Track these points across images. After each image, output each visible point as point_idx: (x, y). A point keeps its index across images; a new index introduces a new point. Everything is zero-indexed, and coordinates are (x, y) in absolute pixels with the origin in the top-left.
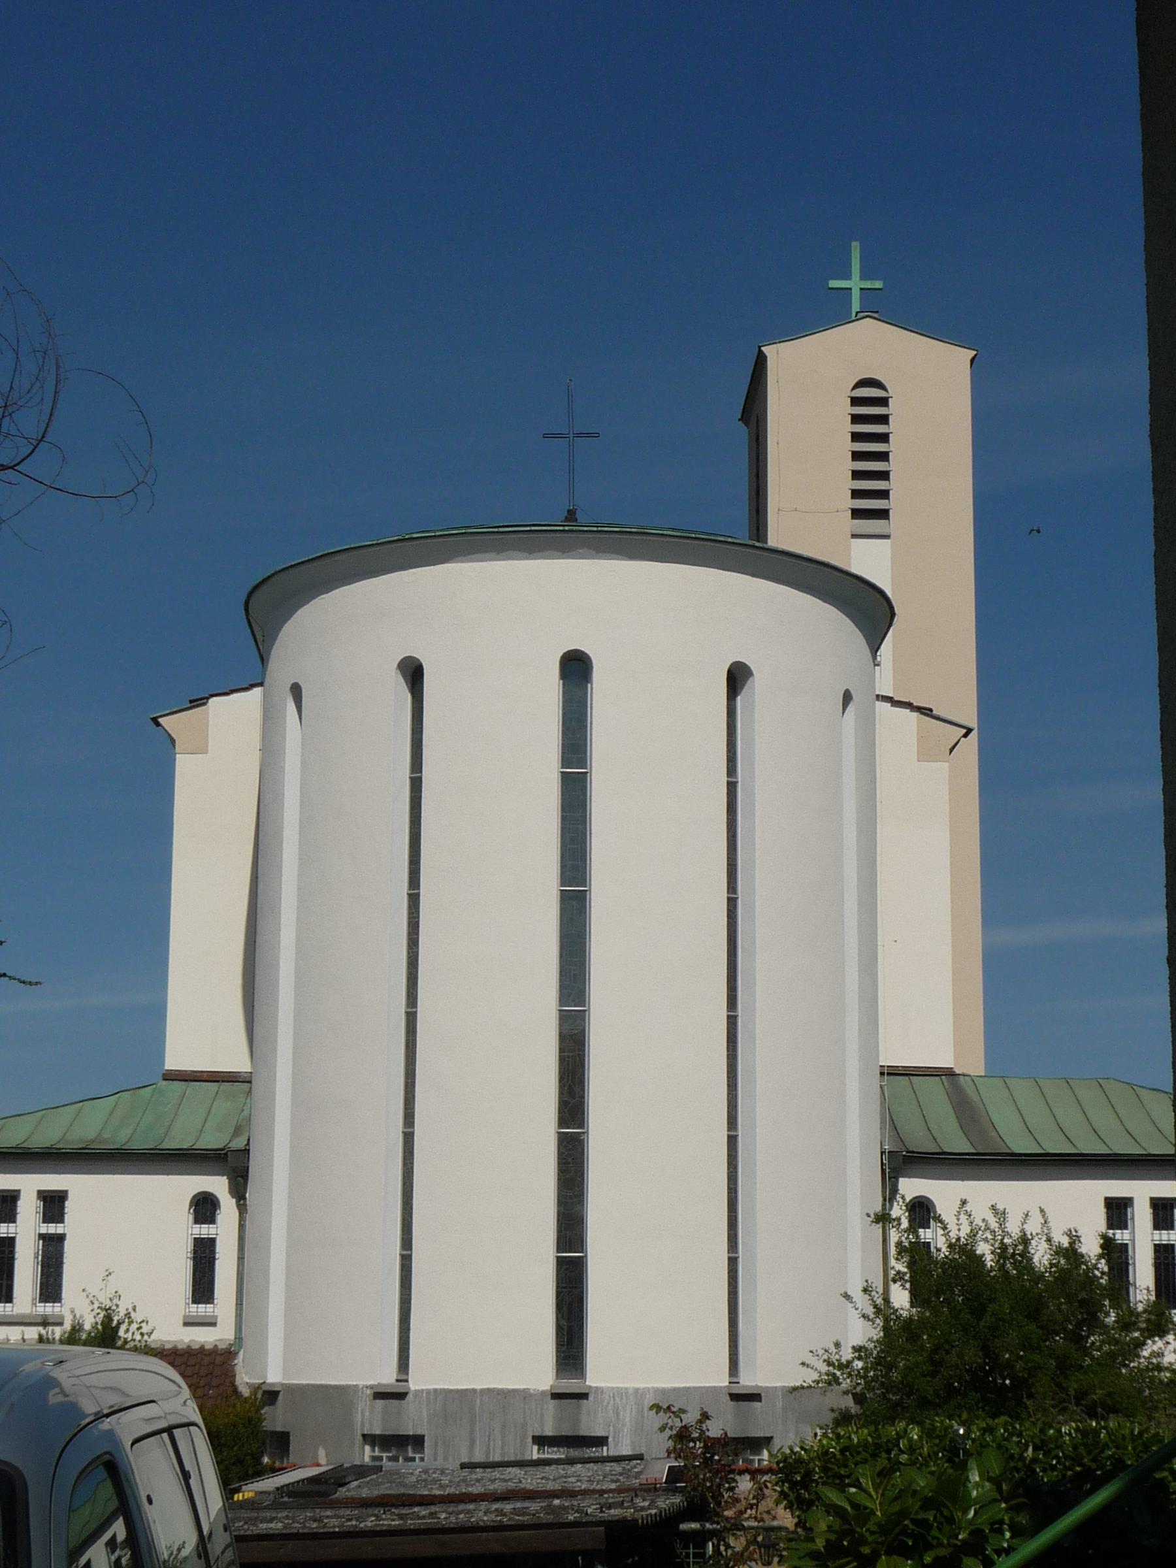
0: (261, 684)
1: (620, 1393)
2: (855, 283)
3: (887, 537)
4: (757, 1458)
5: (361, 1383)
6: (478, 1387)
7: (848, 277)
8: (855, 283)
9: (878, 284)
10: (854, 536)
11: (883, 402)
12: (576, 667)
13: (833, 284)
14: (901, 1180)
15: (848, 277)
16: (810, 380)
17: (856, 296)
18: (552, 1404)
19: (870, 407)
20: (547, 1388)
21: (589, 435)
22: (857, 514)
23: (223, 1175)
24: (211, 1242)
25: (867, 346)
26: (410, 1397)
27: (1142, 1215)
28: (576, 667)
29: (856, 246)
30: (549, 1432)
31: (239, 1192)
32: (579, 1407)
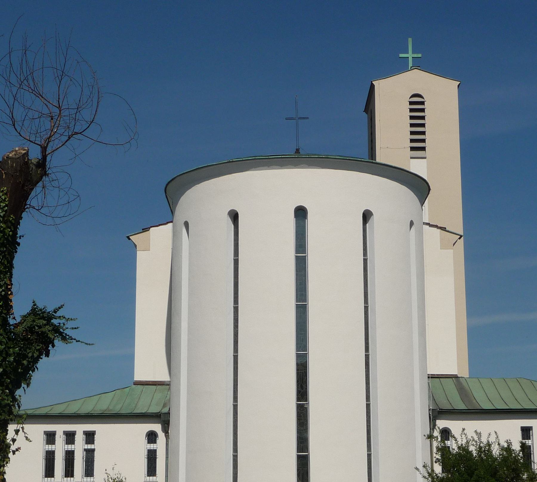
0: (172, 222)
3: (425, 158)
8: (410, 55)
9: (420, 55)
10: (411, 158)
11: (423, 103)
12: (301, 213)
13: (401, 55)
16: (392, 94)
17: (410, 60)
19: (417, 105)
21: (304, 118)
25: (415, 80)
28: (301, 213)
29: (410, 40)
31: (166, 430)
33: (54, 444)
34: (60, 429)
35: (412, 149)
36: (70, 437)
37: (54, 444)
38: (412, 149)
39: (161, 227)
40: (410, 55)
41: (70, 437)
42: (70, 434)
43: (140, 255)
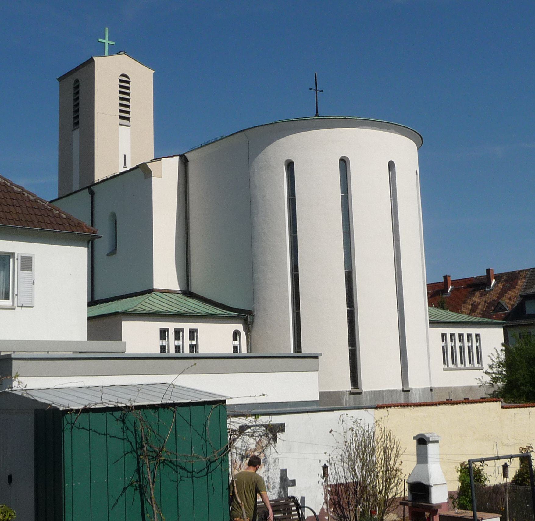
1: (416, 389)
2: (107, 41)
3: (129, 126)
5: (344, 390)
6: (384, 389)
7: (109, 40)
9: (113, 43)
10: (120, 125)
12: (391, 165)
18: (403, 393)
19: (125, 83)
22: (121, 117)
23: (121, 323)
25: (123, 63)
26: (363, 394)
28: (391, 165)
29: (107, 29)
31: (248, 331)
34: (172, 326)
39: (169, 158)
40: (107, 41)
41: (178, 333)
43: (155, 180)
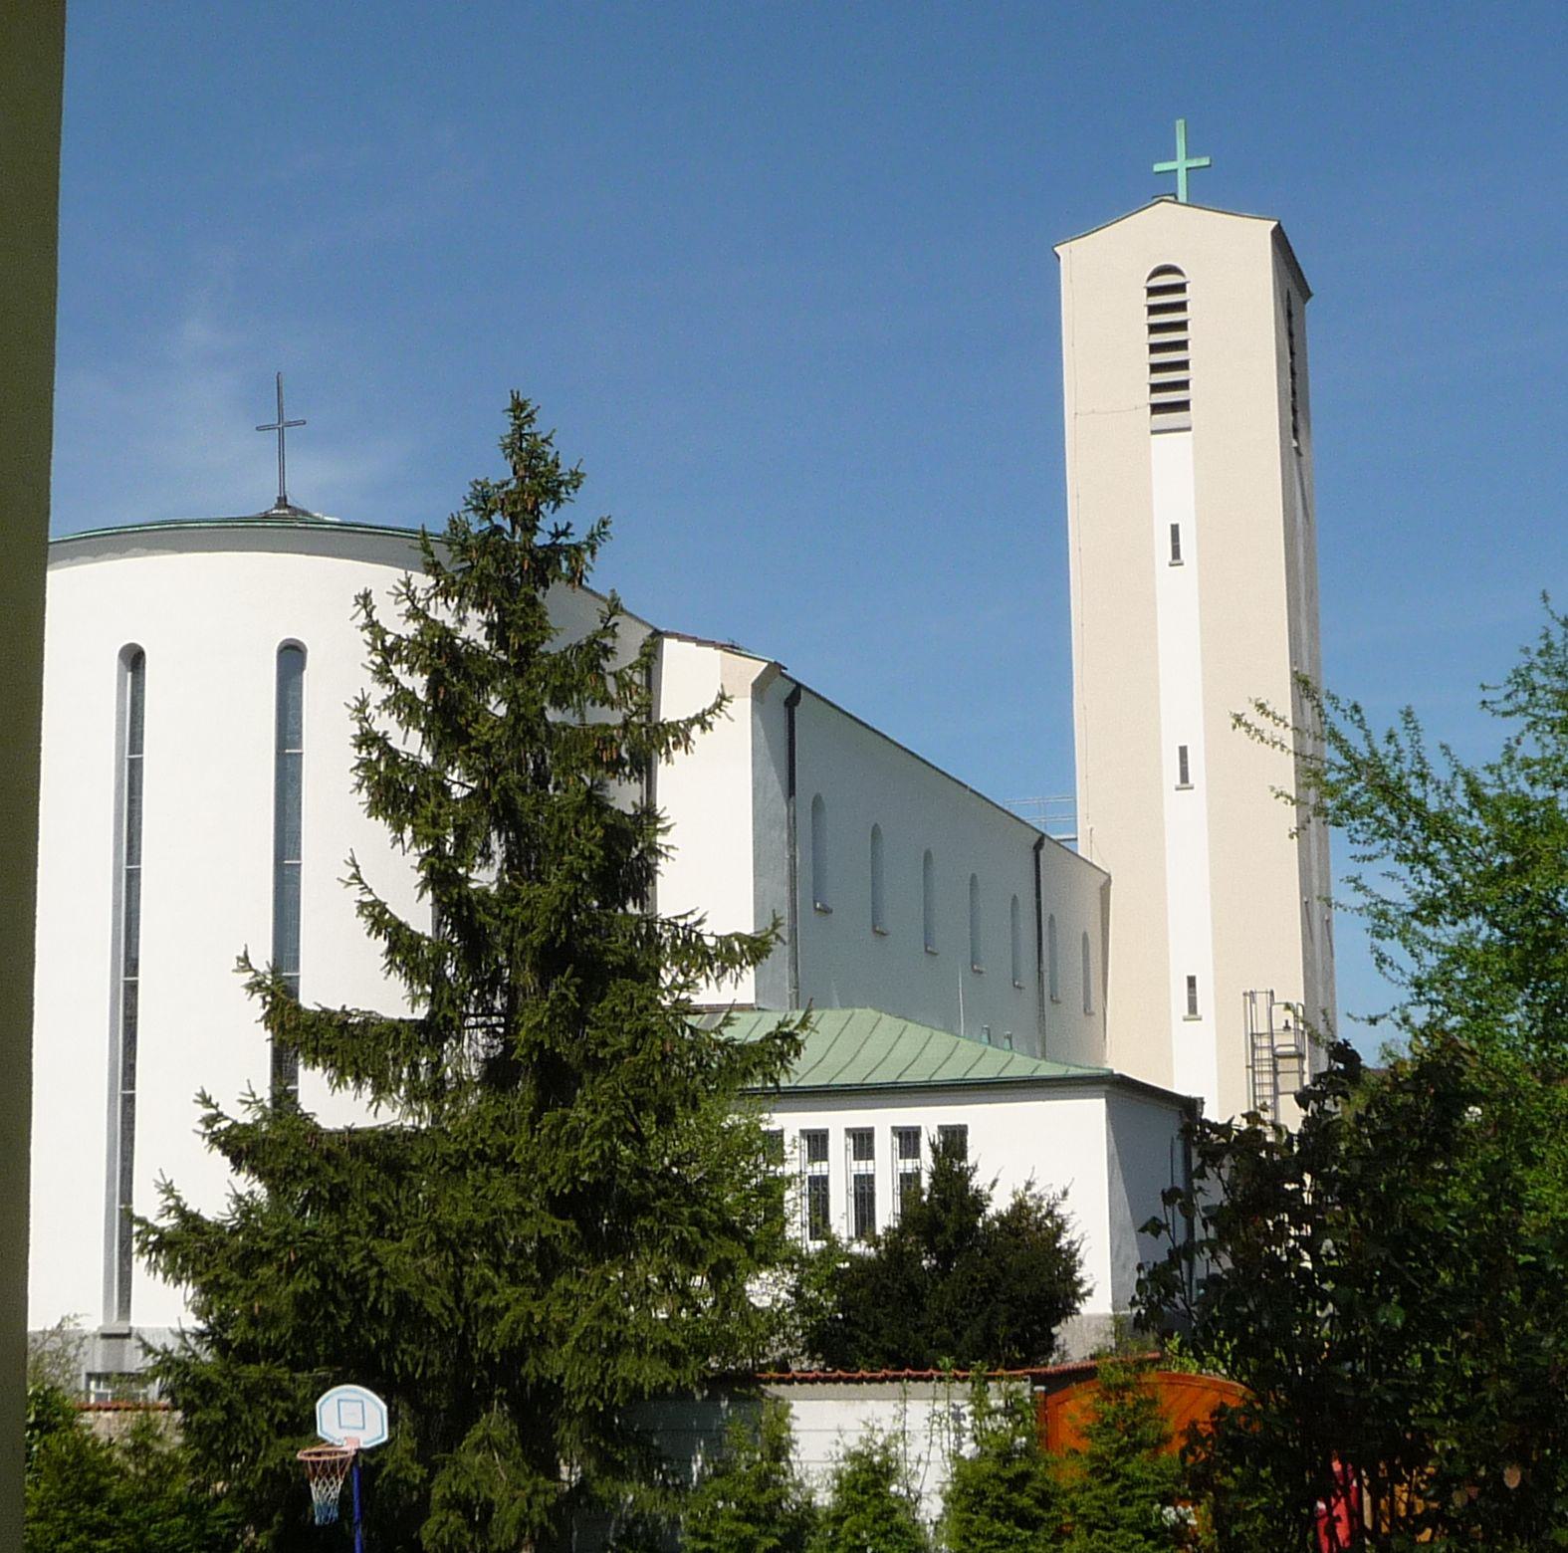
0: (657, 635)
3: (1188, 429)
4: (143, 1391)
7: (1174, 158)
8: (1181, 164)
9: (1205, 162)
10: (1153, 432)
11: (1180, 288)
13: (1158, 167)
14: (1102, 1102)
15: (1174, 158)
16: (1100, 277)
17: (1182, 176)
18: (101, 1343)
19: (1167, 297)
20: (95, 1329)
21: (296, 423)
24: (870, 1178)
27: (885, 1145)
28: (134, 659)
29: (1180, 124)
30: (99, 1369)
32: (123, 1346)
33: (825, 1158)
35: (1156, 408)
36: (863, 1143)
37: (825, 1158)
38: (1156, 408)
42: (908, 1134)
